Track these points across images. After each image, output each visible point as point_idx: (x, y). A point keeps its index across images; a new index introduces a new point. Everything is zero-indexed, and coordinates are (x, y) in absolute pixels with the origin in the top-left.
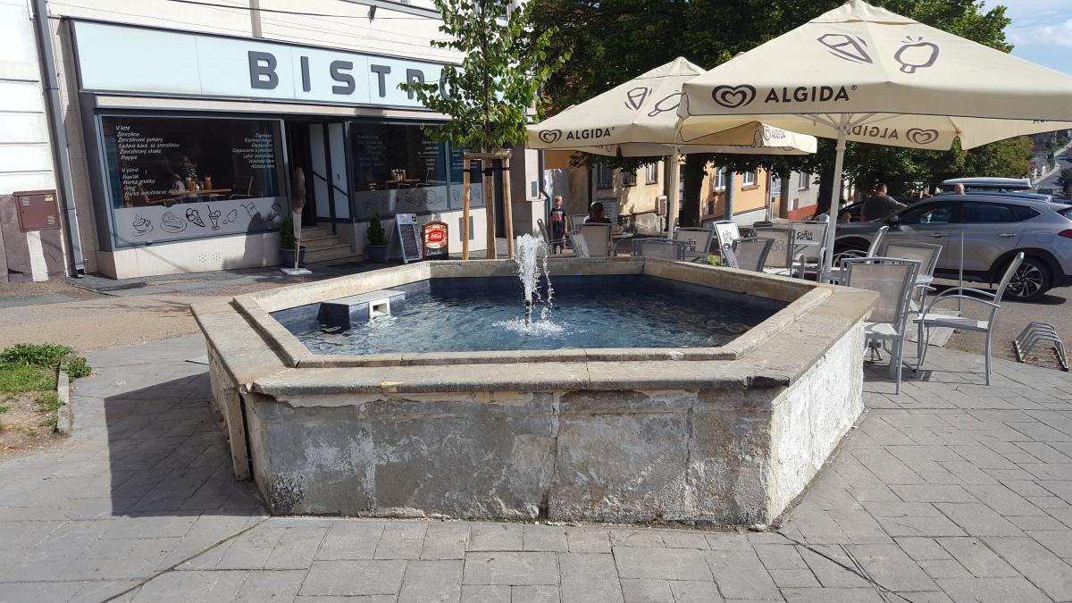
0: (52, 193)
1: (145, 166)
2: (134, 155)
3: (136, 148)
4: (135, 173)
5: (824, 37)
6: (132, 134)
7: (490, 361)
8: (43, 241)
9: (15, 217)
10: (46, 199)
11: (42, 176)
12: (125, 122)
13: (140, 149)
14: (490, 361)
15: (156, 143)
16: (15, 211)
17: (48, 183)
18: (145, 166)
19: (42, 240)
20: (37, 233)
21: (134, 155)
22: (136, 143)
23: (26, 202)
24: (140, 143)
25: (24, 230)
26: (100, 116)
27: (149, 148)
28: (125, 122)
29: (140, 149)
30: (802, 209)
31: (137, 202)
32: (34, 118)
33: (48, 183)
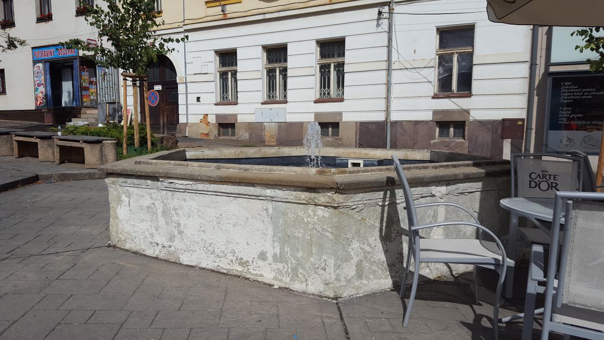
0: (523, 120)
1: (575, 105)
2: (571, 99)
3: (573, 95)
4: (569, 110)
5: (184, 18)
6: (572, 87)
7: (201, 194)
8: (512, 144)
9: (500, 131)
10: (99, 126)
11: (519, 111)
12: (569, 80)
13: (575, 96)
14: (201, 194)
15: (589, 92)
16: (500, 128)
17: (523, 115)
18: (575, 105)
19: (511, 144)
20: (509, 140)
21: (571, 99)
22: (574, 92)
23: (507, 124)
24: (577, 92)
25: (503, 138)
26: (552, 77)
27: (583, 95)
28: (569, 80)
29: (575, 96)
30: (382, 191)
31: (568, 127)
32: (522, 81)
33: (523, 115)
